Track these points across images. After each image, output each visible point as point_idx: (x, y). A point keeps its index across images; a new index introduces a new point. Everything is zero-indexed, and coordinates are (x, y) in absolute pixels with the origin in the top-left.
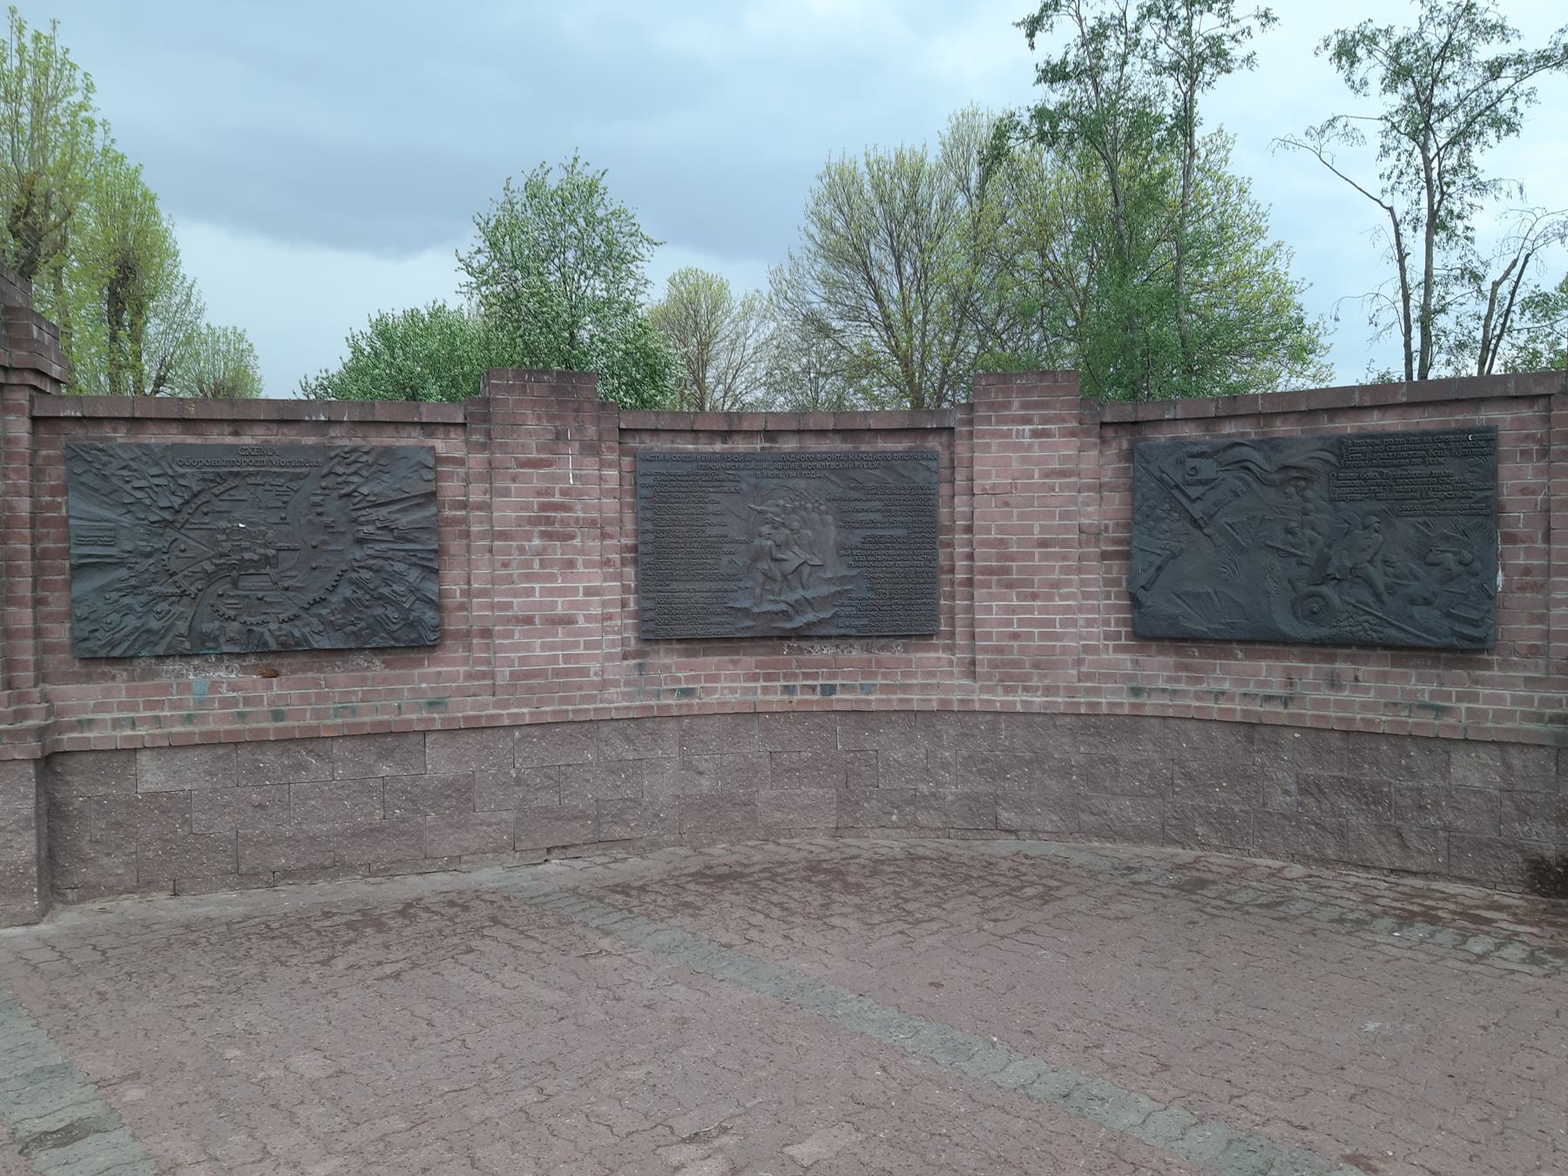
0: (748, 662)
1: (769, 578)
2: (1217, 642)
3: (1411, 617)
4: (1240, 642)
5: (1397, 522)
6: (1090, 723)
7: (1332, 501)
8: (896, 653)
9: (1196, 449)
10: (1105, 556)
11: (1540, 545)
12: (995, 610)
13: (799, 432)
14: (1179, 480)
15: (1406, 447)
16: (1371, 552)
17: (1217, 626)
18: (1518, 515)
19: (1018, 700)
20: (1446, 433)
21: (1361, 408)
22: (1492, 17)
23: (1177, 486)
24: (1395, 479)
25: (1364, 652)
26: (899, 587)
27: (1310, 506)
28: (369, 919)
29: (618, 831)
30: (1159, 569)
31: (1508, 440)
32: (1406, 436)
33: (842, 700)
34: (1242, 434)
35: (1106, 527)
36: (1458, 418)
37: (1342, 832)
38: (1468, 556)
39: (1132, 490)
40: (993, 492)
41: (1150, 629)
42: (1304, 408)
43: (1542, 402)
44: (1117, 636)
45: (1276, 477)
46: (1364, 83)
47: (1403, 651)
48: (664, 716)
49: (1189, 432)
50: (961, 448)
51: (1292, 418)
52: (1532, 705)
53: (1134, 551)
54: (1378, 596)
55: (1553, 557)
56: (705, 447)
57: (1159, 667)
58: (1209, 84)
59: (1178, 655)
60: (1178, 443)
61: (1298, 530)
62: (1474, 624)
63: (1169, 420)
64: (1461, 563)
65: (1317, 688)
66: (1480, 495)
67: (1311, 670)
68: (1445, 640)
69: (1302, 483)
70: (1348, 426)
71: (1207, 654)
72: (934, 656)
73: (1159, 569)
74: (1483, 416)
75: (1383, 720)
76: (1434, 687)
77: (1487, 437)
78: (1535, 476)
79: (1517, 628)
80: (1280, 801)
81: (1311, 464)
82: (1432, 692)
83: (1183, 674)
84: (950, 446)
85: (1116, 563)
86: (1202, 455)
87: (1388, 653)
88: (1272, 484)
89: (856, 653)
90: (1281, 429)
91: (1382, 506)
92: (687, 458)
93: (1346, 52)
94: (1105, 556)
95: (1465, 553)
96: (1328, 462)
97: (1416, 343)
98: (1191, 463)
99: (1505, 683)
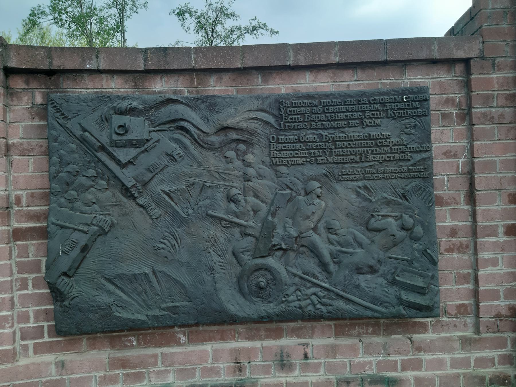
3: (358, 287)
4: (180, 326)
5: (338, 187)
7: (273, 166)
9: (124, 105)
10: (18, 235)
14: (105, 140)
15: (343, 108)
16: (316, 218)
17: (157, 312)
20: (381, 94)
22: (230, 11)
23: (103, 148)
24: (334, 141)
25: (309, 324)
27: (251, 171)
30: (85, 249)
34: (175, 92)
35: (18, 200)
38: (409, 221)
39: (49, 153)
42: (239, 66)
43: (459, 68)
44: (39, 332)
45: (215, 139)
46: (189, 28)
47: (343, 322)
51: (226, 77)
52: (468, 366)
53: (52, 229)
54: (324, 266)
58: (129, 17)
59: (113, 347)
60: (103, 98)
61: (241, 198)
62: (421, 291)
63: (91, 72)
64: (403, 228)
65: (266, 370)
66: (418, 157)
68: (392, 310)
69: (242, 147)
70: (281, 86)
71: (147, 342)
73: (85, 249)
76: (381, 358)
79: (452, 292)
81: (253, 125)
82: (379, 363)
83: (120, 372)
85: (33, 245)
86: (131, 111)
87: (332, 323)
88: (211, 147)
90: (215, 87)
91: (321, 170)
93: (181, 14)
94: (18, 235)
95: (406, 217)
96: (267, 123)
98: (118, 120)
99: (446, 346)
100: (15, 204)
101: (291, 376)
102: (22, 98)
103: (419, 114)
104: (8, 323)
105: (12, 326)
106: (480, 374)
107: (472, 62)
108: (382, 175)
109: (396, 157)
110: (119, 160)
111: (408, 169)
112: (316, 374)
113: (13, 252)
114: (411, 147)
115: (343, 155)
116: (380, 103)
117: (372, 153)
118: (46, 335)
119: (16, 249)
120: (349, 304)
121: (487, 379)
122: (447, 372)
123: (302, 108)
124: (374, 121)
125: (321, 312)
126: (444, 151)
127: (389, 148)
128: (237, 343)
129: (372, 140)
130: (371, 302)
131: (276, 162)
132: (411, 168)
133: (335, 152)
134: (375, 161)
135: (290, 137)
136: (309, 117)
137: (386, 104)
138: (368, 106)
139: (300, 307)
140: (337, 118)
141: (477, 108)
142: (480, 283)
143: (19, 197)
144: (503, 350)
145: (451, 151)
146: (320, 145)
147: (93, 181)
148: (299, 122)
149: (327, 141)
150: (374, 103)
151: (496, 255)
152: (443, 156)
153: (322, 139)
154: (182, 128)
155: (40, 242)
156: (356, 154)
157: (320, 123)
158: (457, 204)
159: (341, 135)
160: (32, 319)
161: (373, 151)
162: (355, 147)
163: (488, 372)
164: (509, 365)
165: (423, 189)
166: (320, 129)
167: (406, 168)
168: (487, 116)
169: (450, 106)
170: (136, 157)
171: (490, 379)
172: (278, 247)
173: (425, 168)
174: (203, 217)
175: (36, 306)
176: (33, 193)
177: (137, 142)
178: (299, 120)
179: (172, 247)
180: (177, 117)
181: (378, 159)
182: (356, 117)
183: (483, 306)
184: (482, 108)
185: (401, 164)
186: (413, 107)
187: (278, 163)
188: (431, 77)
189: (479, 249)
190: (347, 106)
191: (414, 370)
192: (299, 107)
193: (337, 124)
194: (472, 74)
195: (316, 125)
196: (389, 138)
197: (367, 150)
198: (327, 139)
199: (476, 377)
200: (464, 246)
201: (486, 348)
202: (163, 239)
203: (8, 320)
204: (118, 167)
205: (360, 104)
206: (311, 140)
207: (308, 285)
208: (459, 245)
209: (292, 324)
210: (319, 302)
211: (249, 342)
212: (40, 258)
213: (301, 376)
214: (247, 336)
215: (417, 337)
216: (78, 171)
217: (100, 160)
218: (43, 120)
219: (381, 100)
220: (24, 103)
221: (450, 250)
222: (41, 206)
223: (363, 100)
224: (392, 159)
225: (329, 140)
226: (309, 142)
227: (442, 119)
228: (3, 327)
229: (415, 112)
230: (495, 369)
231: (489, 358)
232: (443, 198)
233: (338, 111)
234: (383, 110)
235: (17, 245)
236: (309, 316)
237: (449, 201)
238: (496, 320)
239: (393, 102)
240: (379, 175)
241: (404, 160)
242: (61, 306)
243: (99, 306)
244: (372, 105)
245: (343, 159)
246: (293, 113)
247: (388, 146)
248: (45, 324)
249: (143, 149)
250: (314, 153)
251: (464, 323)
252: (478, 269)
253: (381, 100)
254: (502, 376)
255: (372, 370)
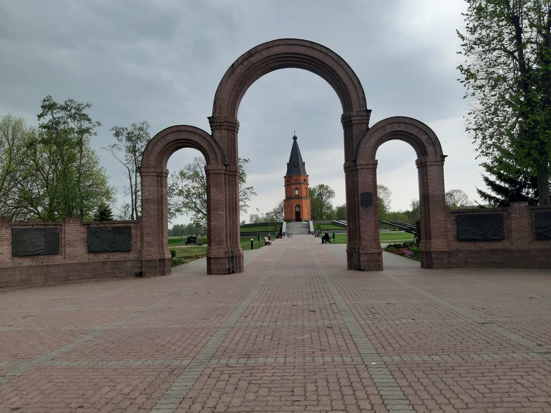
0: (30, 259)
1: (33, 246)
2: (99, 252)
6: (82, 264)
8: (53, 256)
12: (68, 250)
18: (133, 235)
19: (72, 262)
26: (54, 247)
29: (10, 285)
31: (132, 227)
32: (121, 227)
33: (45, 264)
36: (127, 225)
37: (115, 274)
40: (68, 233)
41: (90, 251)
47: (122, 251)
48: (18, 267)
49: (95, 225)
50: (63, 227)
56: (23, 227)
57: (92, 256)
60: (94, 227)
67: (111, 255)
70: (115, 225)
72: (59, 257)
74: (130, 225)
75: (119, 260)
77: (130, 227)
79: (134, 248)
80: (108, 271)
84: (61, 227)
89: (46, 257)
92: (20, 229)
97: (134, 198)
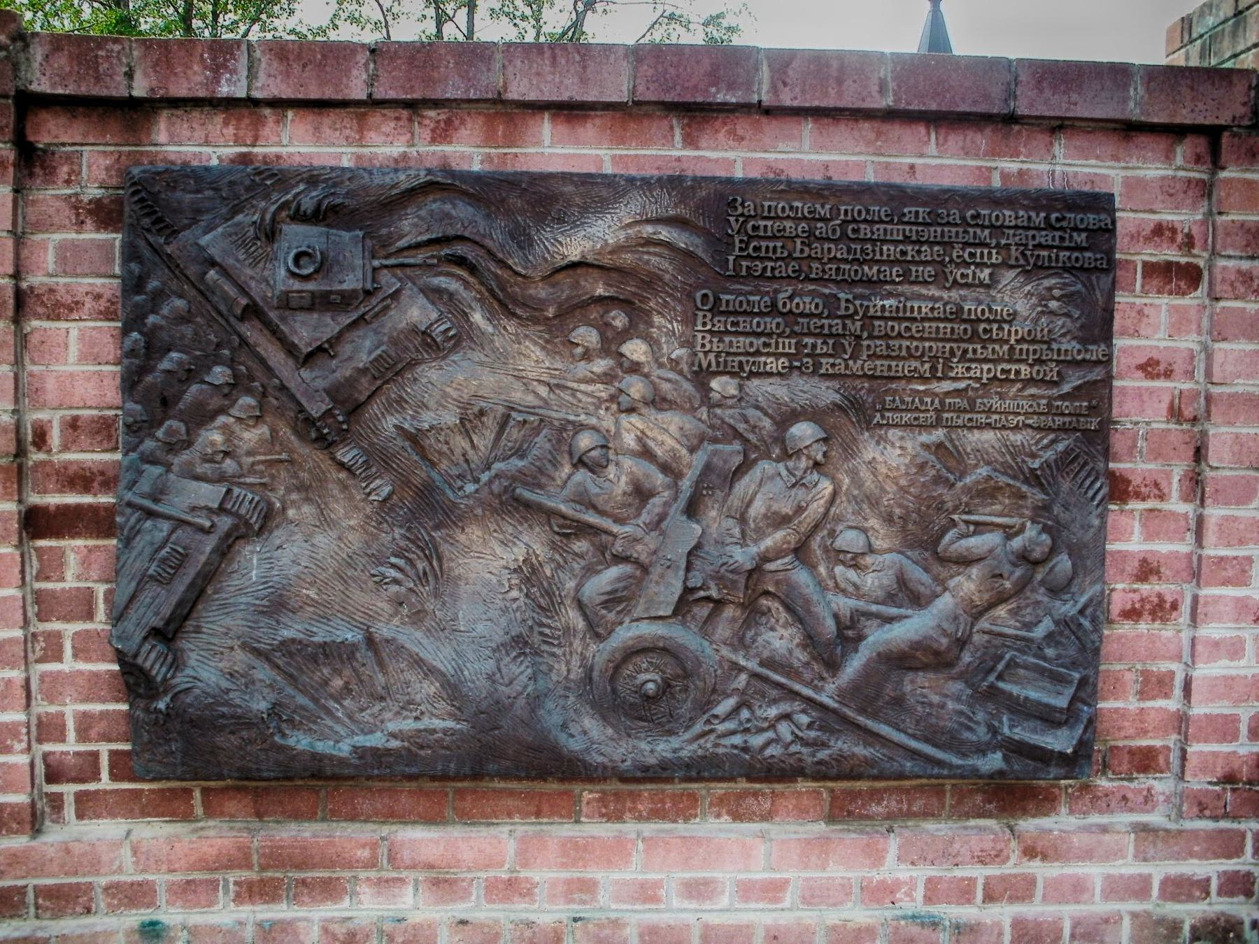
11: (1177, 505)
13: (413, 106)
21: (768, 112)
28: (1004, 123)
55: (1210, 536)
69: (619, 320)
78: (1176, 329)
100: (35, 444)
101: (709, 908)
102: (55, 168)
103: (1086, 266)
104: (20, 741)
105: (29, 749)
106: (1171, 916)
107: (1225, 138)
108: (984, 416)
109: (1023, 373)
110: (295, 346)
111: (1049, 405)
112: (774, 906)
113: (28, 569)
114: (1063, 347)
115: (888, 357)
116: (992, 226)
117: (963, 358)
118: (105, 775)
119: (34, 558)
120: (871, 745)
121: (1187, 928)
122: (1092, 908)
123: (788, 224)
124: (974, 273)
125: (800, 760)
126: (1143, 360)
127: (1006, 347)
128: (577, 827)
129: (965, 321)
130: (927, 740)
131: (709, 365)
132: (1060, 403)
133: (869, 346)
134: (970, 378)
135: (752, 298)
136: (806, 249)
137: (1007, 231)
138: (961, 230)
139: (745, 749)
140: (878, 257)
141: (1230, 257)
142: (1195, 697)
143: (42, 427)
144: (1233, 861)
145: (1158, 363)
146: (830, 326)
147: (225, 396)
148: (778, 259)
149: (851, 317)
150: (977, 225)
151: (1239, 633)
152: (1140, 374)
153: (838, 308)
154: (461, 261)
155: (91, 542)
156: (923, 355)
157: (834, 267)
158: (1162, 497)
159: (887, 303)
160: (71, 735)
161: (965, 351)
162: (922, 339)
163: (1190, 912)
164: (1242, 898)
165: (1081, 461)
166: (834, 281)
167: (1044, 401)
168: (1251, 279)
169: (1165, 245)
170: (340, 336)
171: (1194, 928)
172: (702, 594)
173: (1089, 408)
174: (501, 503)
175: (87, 700)
176: (75, 419)
177: (343, 297)
178: (778, 255)
179: (420, 579)
180: (451, 232)
181: (978, 375)
182: (929, 258)
183: (1195, 753)
184: (1241, 258)
185: (1033, 391)
186: (1074, 241)
187: (714, 368)
188: (1123, 165)
189: (1200, 617)
190: (907, 228)
191: (1013, 899)
192: (777, 218)
193: (879, 271)
194: (1223, 168)
195: (824, 271)
196: (1010, 322)
197: (951, 348)
198: (851, 311)
199: (1161, 921)
200: (1168, 605)
201: (1192, 855)
202: (396, 556)
203: (20, 733)
204: (291, 362)
205: (940, 224)
206: (807, 311)
207: (774, 693)
208: (1156, 600)
209: (720, 788)
210: (797, 736)
211: (609, 825)
212: (90, 585)
213: (737, 910)
214: (604, 811)
215: (1029, 825)
216: (190, 370)
217: (244, 341)
218: (106, 229)
219: (993, 219)
220: (60, 182)
221: (1132, 614)
222: (93, 451)
223: (948, 215)
224: (1012, 376)
225: (856, 312)
226: (802, 315)
227: (1144, 277)
228: (8, 750)
229: (1077, 259)
230: (1210, 904)
231: (1195, 878)
232: (1129, 482)
233: (882, 237)
234: (998, 246)
235: (36, 549)
236: (769, 770)
237: (1143, 489)
238: (1224, 789)
239: (1023, 228)
240: (979, 416)
241: (1042, 381)
242: (147, 710)
243: (239, 717)
244: (971, 230)
245: (890, 366)
246: (762, 234)
247: (1007, 342)
248: (104, 749)
249: (354, 316)
250: (814, 346)
251: (1145, 793)
252: (1193, 663)
253: (993, 219)
254: (1222, 922)
255: (913, 900)
